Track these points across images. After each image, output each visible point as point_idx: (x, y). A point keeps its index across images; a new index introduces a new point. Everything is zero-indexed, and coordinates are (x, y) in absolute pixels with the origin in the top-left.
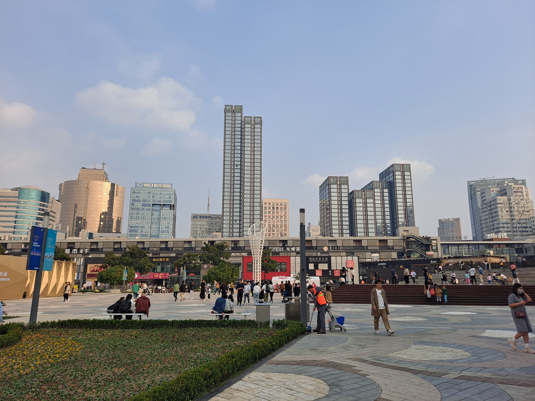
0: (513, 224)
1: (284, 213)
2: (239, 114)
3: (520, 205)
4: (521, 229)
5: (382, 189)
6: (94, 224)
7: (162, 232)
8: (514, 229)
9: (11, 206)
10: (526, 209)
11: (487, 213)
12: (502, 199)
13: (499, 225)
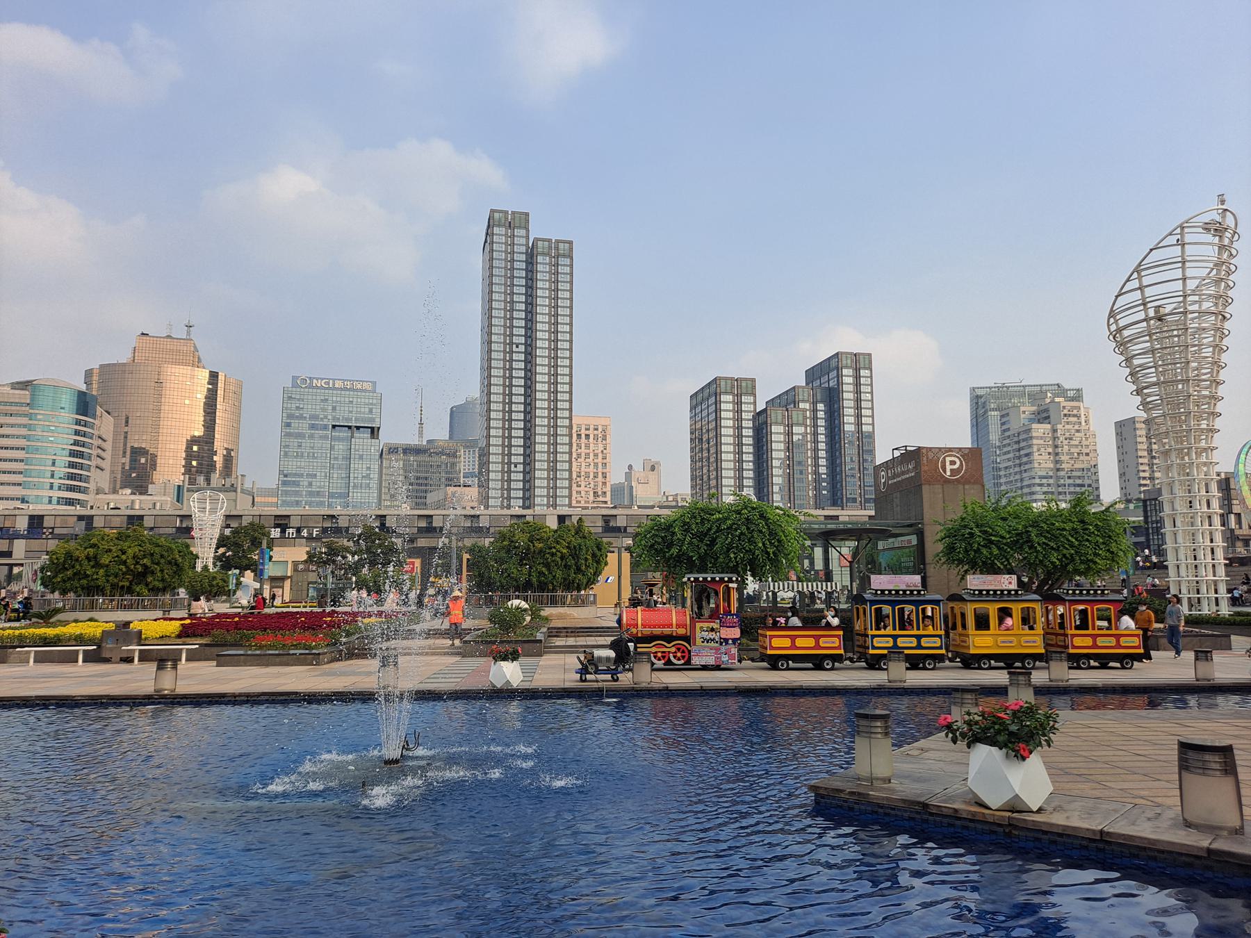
0: (1058, 478)
2: (523, 232)
3: (1073, 442)
6: (171, 467)
7: (355, 487)
8: (1060, 489)
9: (12, 426)
10: (1085, 451)
11: (1011, 455)
12: (1040, 429)
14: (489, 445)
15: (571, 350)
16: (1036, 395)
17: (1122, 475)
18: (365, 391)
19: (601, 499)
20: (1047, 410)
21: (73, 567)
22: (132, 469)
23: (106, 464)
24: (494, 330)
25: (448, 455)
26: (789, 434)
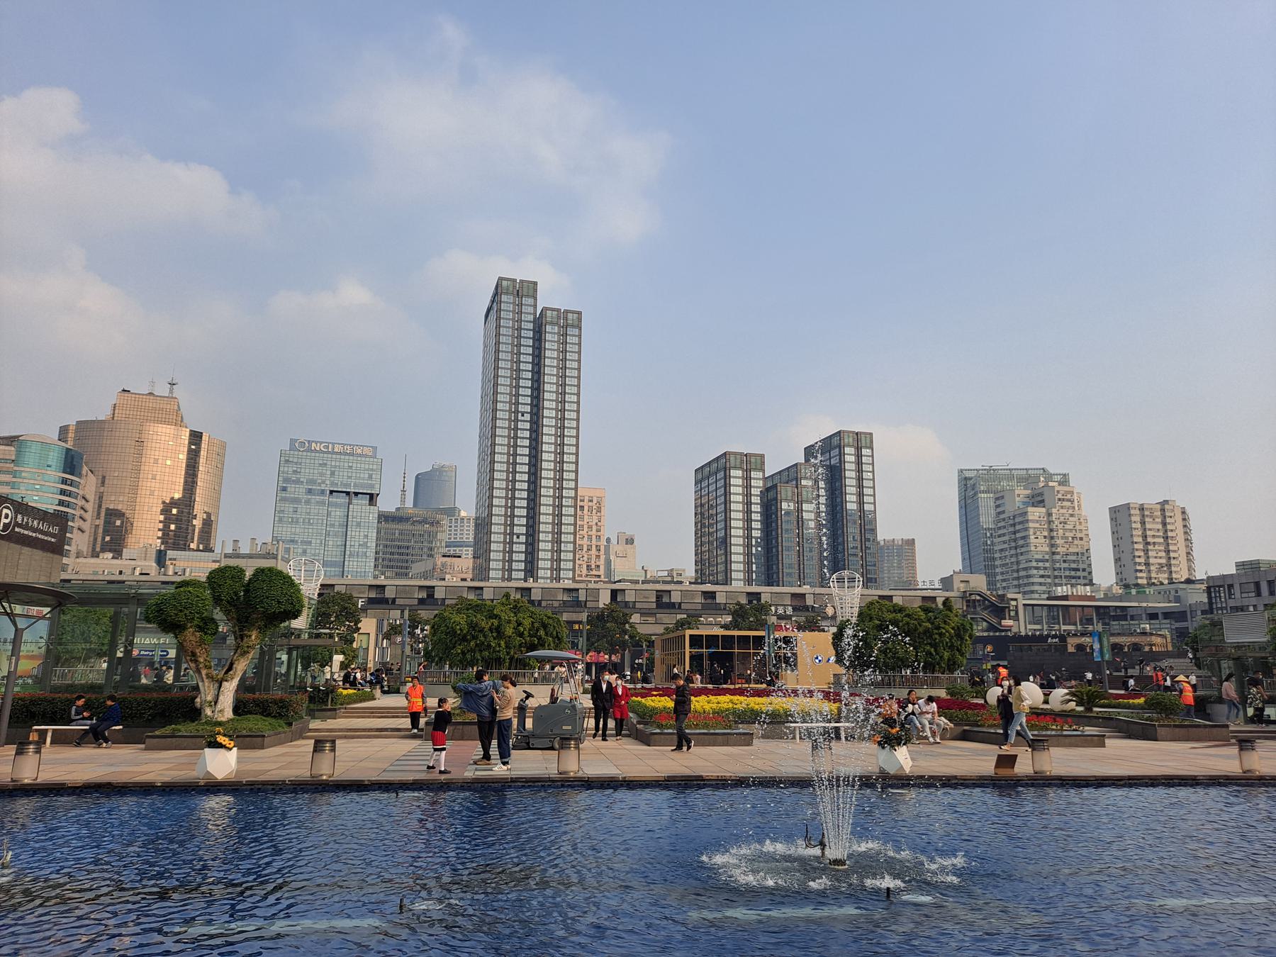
0: (1054, 561)
1: (595, 521)
2: (531, 301)
3: (1067, 527)
4: (1067, 573)
6: (147, 531)
10: (1079, 535)
11: (1007, 538)
12: (1035, 513)
14: (491, 515)
15: (578, 420)
16: (1027, 478)
17: (1117, 560)
18: (366, 456)
19: (594, 572)
20: (1041, 494)
23: (86, 526)
25: (432, 524)
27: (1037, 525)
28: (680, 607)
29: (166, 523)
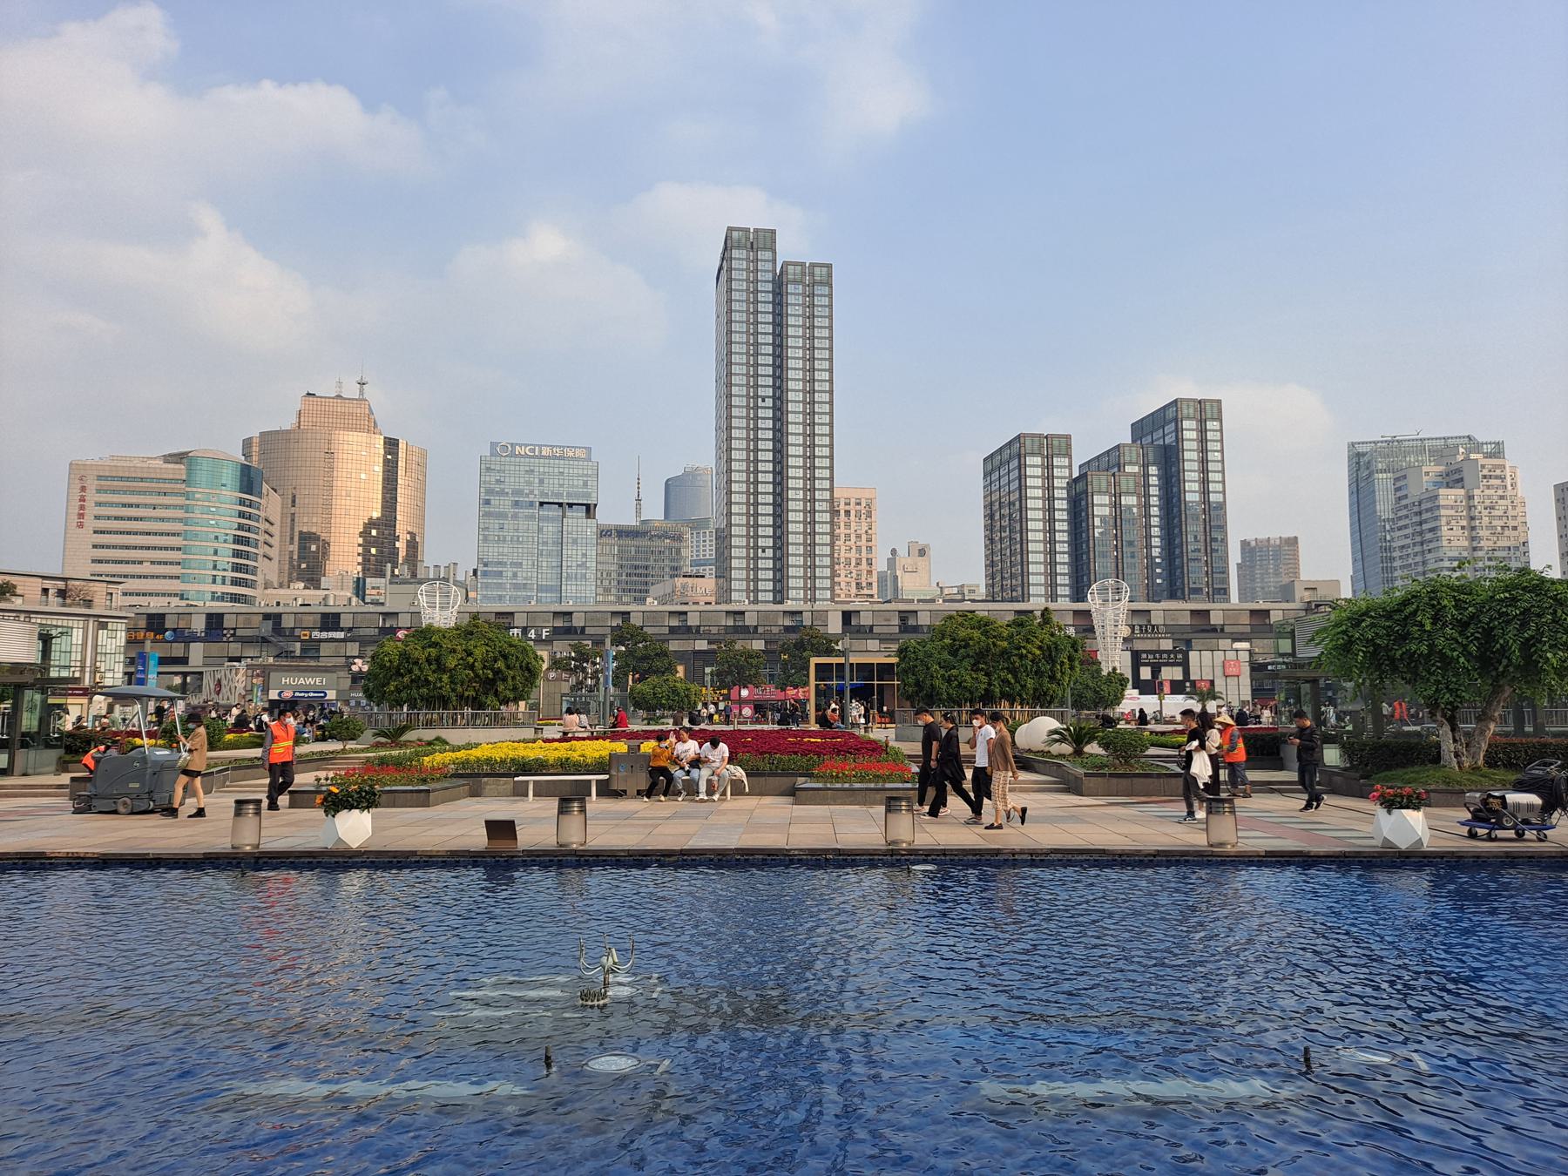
2: (768, 255)
5: (1145, 466)
6: (345, 558)
9: (167, 507)
10: (1511, 523)
11: (1409, 531)
13: (1441, 564)
14: (730, 525)
16: (1442, 450)
18: (578, 459)
19: (866, 592)
20: (1459, 471)
21: (410, 672)
22: (301, 558)
23: (274, 553)
24: (735, 380)
25: (673, 538)
26: (1116, 505)
27: (1452, 512)
28: (698, 631)
29: (366, 546)
